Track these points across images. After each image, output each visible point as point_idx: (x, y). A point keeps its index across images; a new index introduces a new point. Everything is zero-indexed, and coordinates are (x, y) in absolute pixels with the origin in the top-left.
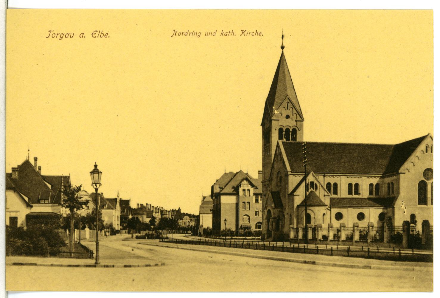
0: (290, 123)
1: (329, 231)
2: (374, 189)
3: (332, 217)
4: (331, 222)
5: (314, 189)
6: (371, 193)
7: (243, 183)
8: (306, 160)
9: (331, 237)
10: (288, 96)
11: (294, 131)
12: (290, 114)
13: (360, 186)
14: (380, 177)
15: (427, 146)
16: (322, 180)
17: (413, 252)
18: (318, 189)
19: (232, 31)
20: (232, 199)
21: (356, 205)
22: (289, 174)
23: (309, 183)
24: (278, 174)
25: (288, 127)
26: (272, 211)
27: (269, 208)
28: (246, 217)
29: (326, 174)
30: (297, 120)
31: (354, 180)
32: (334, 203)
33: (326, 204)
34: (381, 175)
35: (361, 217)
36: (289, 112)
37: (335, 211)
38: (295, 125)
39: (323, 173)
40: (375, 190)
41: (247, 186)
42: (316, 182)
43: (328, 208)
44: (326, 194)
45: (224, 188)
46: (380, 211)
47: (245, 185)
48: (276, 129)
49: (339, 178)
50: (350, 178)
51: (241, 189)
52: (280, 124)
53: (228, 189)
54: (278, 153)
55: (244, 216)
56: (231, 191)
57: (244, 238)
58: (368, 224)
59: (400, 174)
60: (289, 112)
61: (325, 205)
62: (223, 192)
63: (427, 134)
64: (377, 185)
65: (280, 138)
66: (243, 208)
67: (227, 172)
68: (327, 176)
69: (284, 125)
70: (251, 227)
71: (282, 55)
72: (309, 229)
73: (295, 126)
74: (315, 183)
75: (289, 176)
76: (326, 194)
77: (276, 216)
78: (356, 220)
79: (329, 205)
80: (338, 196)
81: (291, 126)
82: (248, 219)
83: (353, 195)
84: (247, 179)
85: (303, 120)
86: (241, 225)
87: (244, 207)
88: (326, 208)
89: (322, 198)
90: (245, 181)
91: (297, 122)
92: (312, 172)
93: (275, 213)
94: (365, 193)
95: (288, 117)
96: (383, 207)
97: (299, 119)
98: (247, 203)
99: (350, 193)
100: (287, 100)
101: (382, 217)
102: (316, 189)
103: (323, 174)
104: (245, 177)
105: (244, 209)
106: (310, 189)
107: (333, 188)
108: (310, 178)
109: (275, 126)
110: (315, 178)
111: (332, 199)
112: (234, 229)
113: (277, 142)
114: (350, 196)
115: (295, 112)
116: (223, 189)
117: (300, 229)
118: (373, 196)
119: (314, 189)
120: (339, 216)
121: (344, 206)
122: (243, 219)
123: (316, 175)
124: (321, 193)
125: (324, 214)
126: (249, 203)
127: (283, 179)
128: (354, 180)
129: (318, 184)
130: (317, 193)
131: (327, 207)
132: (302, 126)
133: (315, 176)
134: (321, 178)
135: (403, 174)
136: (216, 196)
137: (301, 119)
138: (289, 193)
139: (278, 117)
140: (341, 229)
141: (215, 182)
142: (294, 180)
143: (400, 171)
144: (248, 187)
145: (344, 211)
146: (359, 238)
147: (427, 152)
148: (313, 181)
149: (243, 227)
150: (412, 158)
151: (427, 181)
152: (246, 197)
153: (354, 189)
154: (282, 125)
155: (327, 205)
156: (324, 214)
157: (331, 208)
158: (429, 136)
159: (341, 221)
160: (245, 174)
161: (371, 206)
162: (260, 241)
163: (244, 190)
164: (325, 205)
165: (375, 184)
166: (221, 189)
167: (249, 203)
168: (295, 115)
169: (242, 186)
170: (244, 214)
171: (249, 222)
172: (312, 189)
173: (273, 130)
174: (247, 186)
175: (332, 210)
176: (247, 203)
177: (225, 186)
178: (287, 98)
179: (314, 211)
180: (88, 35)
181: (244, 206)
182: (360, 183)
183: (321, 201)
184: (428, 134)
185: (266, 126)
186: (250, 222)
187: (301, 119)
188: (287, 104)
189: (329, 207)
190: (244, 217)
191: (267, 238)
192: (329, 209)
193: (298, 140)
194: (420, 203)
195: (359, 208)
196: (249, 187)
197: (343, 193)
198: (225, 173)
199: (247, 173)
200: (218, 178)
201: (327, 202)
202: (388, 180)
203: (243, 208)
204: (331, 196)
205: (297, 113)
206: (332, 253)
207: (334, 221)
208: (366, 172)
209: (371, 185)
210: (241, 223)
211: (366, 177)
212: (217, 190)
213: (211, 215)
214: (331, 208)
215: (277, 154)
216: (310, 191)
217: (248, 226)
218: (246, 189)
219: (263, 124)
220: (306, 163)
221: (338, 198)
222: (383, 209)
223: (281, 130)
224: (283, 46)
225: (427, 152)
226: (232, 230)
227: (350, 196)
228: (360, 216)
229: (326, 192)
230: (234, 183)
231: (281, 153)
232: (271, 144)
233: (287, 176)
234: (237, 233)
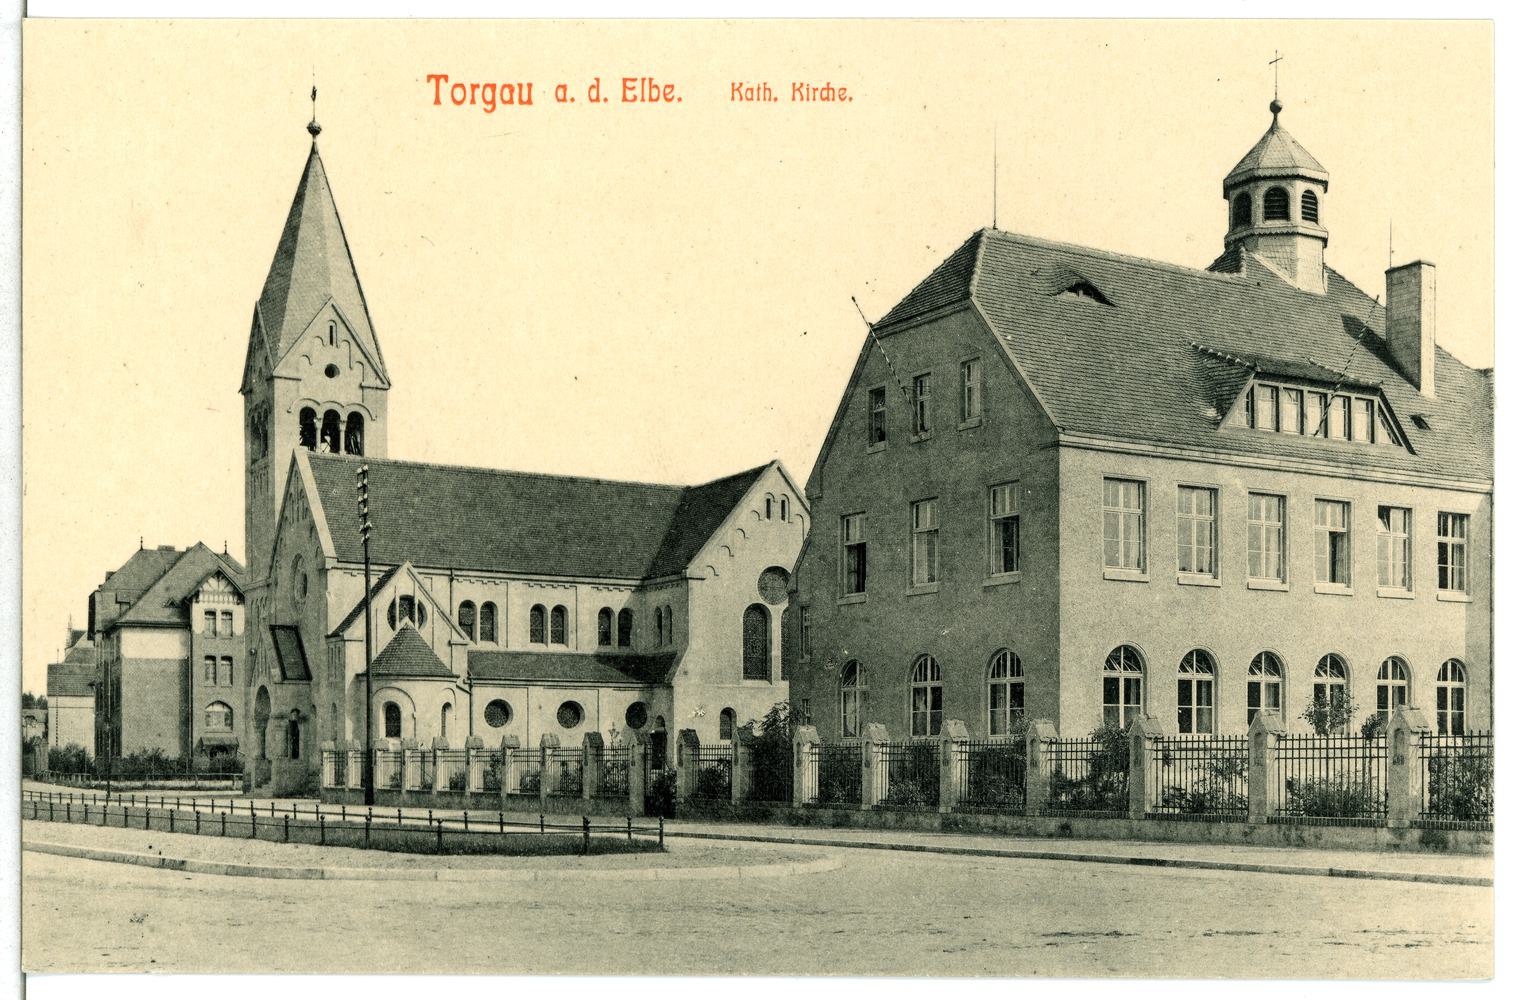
0: (342, 395)
1: (468, 763)
2: (616, 625)
3: (475, 715)
4: (443, 733)
5: (413, 622)
6: (605, 638)
7: (206, 587)
8: (369, 523)
9: (475, 783)
10: (332, 301)
11: (356, 421)
12: (342, 364)
13: (570, 614)
14: (633, 588)
15: (784, 498)
16: (442, 593)
17: (542, 830)
18: (429, 617)
19: (765, 84)
20: (167, 646)
21: (553, 677)
22: (327, 566)
23: (398, 601)
24: (295, 566)
25: (311, 404)
26: (270, 689)
27: (262, 681)
28: (218, 708)
29: (459, 573)
30: (363, 384)
31: (550, 597)
32: (479, 671)
33: (455, 672)
34: (638, 583)
35: (571, 713)
36: (338, 356)
37: (485, 695)
38: (359, 401)
39: (447, 569)
40: (617, 633)
41: (221, 597)
42: (419, 597)
43: (462, 686)
44: (456, 638)
45: (134, 604)
46: (632, 696)
47: (214, 597)
48: (291, 410)
49: (502, 587)
50: (605, 592)
51: (198, 611)
52: (304, 394)
53: (153, 607)
54: (295, 495)
55: (212, 704)
56: (166, 615)
57: (192, 783)
58: (543, 742)
59: (690, 581)
60: (338, 356)
61: (450, 676)
62: (130, 616)
63: (768, 462)
64: (626, 613)
65: (308, 439)
66: (207, 678)
67: (151, 545)
68: (461, 579)
69: (342, 400)
70: (237, 746)
71: (314, 151)
72: (379, 754)
73: (359, 405)
74: (416, 602)
75: (329, 573)
76: (456, 638)
77: (286, 709)
78: (556, 728)
79: (464, 676)
80: (500, 647)
81: (319, 401)
82: (226, 714)
83: (547, 645)
84: (219, 574)
85: (386, 386)
86: (201, 740)
87: (211, 676)
88: (453, 686)
89: (442, 653)
90: (213, 582)
91: (366, 391)
92: (408, 564)
93: (282, 698)
94: (584, 638)
95: (331, 371)
96: (640, 685)
97: (372, 381)
98: (224, 658)
99: (537, 635)
100: (329, 314)
101: (636, 715)
102: (422, 619)
103: (449, 572)
104: (211, 566)
105: (211, 682)
106: (401, 619)
107: (478, 619)
108: (402, 584)
109: (287, 403)
110: (417, 585)
111: (474, 658)
112: (172, 751)
113: (290, 457)
114: (538, 648)
115: (359, 356)
116: (130, 606)
117: (350, 754)
118: (613, 648)
119: (413, 622)
120: (499, 712)
121: (512, 681)
122: (209, 716)
123: (420, 573)
124: (436, 634)
125: (447, 706)
126: (228, 659)
127: (310, 580)
128: (550, 597)
129: (428, 607)
130: (425, 633)
131: (460, 682)
132: (383, 405)
133: (416, 574)
134: (440, 583)
135: (700, 582)
136: (106, 629)
137: (378, 383)
138: (330, 633)
139: (297, 370)
140: (504, 754)
141: (102, 581)
142: (344, 589)
143: (689, 573)
144: (224, 602)
145: (514, 697)
146: (333, 782)
147: (768, 517)
148: (410, 593)
149: (208, 746)
150: (727, 533)
151: (769, 606)
152: (218, 639)
153: (548, 622)
154: (309, 397)
155: (458, 677)
156: (447, 706)
157: (471, 686)
158: (775, 466)
159: (507, 730)
160: (217, 555)
161: (601, 680)
162: (238, 797)
163: (211, 613)
164: (450, 676)
165: (617, 609)
166: (125, 607)
167: (228, 659)
168: (357, 368)
169: (201, 597)
170: (212, 700)
171: (228, 728)
172: (407, 620)
173: (279, 412)
174: (216, 597)
175: (476, 690)
176: (224, 658)
177: (139, 598)
178: (330, 304)
179: (413, 695)
180: (543, 93)
181: (211, 670)
182: (570, 606)
183: (438, 663)
184: (773, 463)
185: (258, 398)
186: (232, 728)
187: (378, 383)
188: (331, 328)
189: (465, 683)
190: (210, 709)
191: (259, 786)
192: (467, 688)
193: (369, 452)
194: (748, 674)
195: (566, 687)
196: (229, 604)
197: (514, 634)
198: (142, 549)
199: (226, 553)
200: (115, 567)
201: (460, 667)
202: (657, 598)
203: (207, 678)
204: (472, 646)
205: (365, 361)
206: (105, 819)
207: (483, 728)
208: (597, 573)
209: (606, 613)
210: (198, 732)
211: (589, 587)
212: (108, 610)
213: (91, 702)
214: (471, 686)
215: (291, 495)
216: (399, 626)
217: (227, 743)
218: (219, 608)
219: (246, 390)
220: (368, 535)
221: (499, 653)
222: (642, 690)
223: (307, 415)
224: (316, 124)
225: (768, 517)
226: (164, 756)
227: (538, 648)
228: (569, 714)
229: (453, 631)
230: (177, 584)
231: (302, 495)
232: (273, 460)
233: (323, 571)
234: (179, 769)
